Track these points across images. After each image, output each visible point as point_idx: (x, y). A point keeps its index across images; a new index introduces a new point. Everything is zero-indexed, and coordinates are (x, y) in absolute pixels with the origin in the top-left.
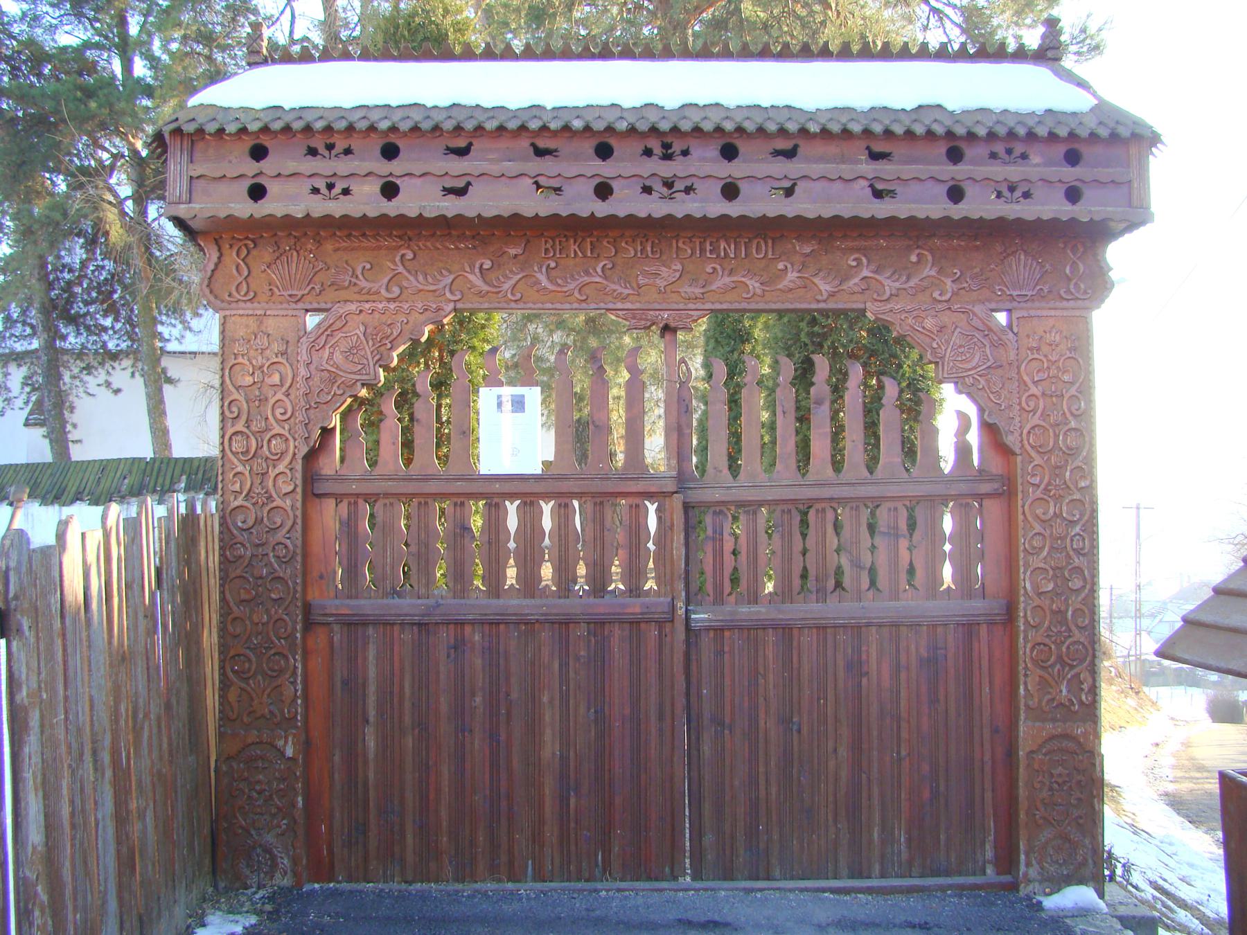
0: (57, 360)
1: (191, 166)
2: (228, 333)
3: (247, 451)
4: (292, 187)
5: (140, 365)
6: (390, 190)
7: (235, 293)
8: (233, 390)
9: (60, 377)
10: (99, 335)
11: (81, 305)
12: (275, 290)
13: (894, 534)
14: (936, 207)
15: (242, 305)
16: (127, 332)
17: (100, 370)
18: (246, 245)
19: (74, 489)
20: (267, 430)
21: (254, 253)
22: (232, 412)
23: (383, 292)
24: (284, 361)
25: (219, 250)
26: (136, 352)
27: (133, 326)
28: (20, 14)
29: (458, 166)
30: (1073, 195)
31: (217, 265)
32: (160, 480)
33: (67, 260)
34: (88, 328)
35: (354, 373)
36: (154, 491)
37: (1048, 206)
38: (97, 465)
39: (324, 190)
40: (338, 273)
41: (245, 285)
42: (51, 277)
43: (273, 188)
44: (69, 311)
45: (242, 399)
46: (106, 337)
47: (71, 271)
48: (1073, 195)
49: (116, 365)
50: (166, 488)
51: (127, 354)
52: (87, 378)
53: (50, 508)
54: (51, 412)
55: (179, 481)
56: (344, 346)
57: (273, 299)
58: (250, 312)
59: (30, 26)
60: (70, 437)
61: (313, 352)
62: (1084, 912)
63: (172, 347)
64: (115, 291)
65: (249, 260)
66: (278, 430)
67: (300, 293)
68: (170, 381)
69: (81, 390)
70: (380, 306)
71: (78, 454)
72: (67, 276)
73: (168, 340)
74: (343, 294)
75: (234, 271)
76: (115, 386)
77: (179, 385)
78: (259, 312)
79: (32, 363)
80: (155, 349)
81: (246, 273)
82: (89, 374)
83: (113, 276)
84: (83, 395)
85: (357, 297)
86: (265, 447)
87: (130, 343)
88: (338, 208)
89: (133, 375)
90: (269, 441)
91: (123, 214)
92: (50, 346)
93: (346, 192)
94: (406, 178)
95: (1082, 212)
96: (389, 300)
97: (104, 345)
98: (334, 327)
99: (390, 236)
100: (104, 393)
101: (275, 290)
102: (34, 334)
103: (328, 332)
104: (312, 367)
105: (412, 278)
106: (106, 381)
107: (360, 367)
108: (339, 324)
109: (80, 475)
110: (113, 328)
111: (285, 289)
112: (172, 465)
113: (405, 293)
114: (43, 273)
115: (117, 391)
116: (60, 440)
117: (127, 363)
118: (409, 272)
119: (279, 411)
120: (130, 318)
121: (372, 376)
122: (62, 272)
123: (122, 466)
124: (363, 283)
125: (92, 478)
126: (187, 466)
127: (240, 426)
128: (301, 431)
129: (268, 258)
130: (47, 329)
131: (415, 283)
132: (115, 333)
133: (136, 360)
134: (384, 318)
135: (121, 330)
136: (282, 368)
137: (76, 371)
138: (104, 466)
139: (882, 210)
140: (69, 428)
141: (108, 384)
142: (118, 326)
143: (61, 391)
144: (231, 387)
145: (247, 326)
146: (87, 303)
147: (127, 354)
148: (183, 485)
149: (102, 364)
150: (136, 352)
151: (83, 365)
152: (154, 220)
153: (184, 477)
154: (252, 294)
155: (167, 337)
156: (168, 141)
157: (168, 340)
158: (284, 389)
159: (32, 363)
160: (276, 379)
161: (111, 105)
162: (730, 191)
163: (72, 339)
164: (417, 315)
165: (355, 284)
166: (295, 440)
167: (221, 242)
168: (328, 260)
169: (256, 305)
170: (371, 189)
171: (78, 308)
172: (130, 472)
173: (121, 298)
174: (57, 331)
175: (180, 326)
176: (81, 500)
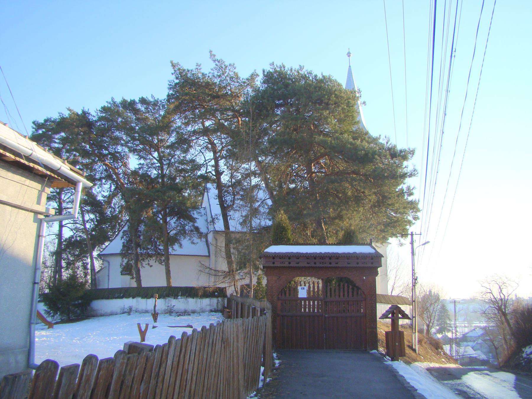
6: (290, 263)
10: (147, 250)
13: (351, 305)
14: (355, 265)
29: (298, 260)
30: (372, 263)
37: (370, 265)
48: (372, 263)
52: (143, 262)
53: (144, 300)
62: (375, 353)
76: (151, 264)
88: (283, 265)
95: (373, 265)
100: (147, 267)
115: (151, 266)
117: (154, 258)
139: (349, 265)
141: (149, 264)
149: (147, 258)
162: (315, 263)
170: (287, 263)
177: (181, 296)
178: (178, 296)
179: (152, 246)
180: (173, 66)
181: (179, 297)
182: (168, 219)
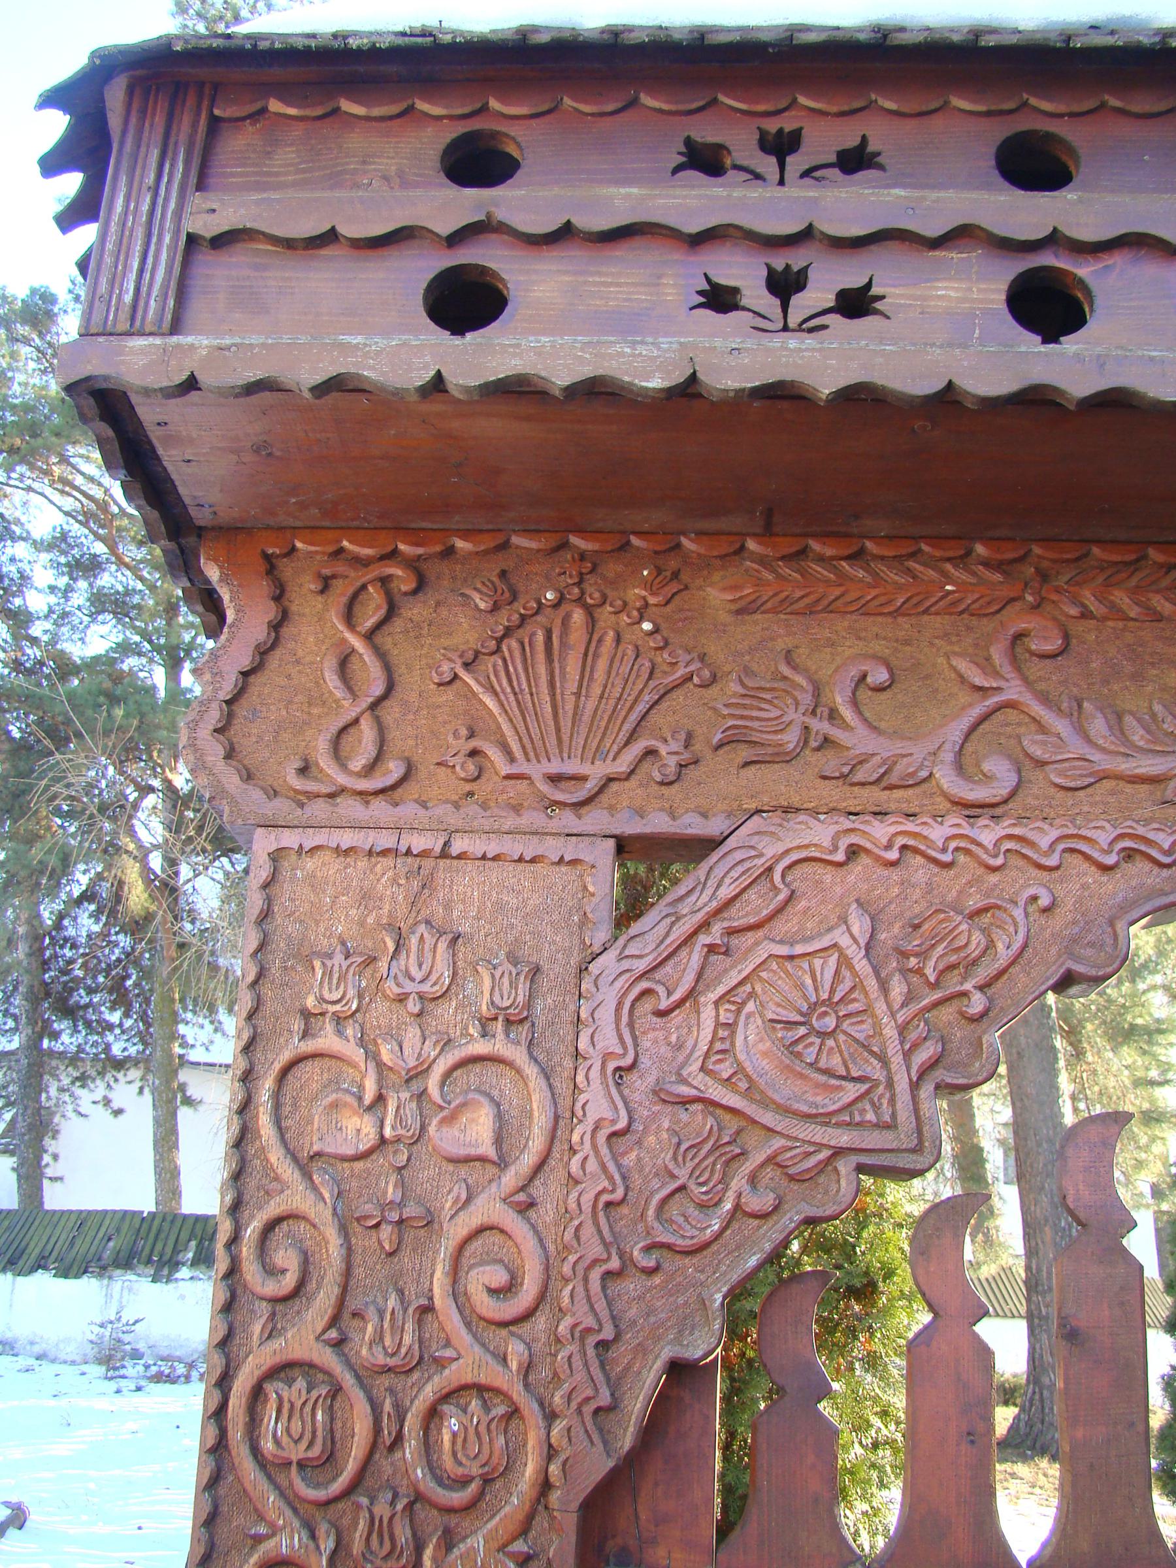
0: (41, 1065)
1: (197, 200)
2: (285, 927)
3: (330, 1459)
4: (623, 279)
5: (150, 1077)
7: (325, 762)
8: (288, 1171)
9: (41, 1089)
11: (82, 991)
12: (494, 754)
15: (350, 808)
16: (140, 1032)
17: (98, 1082)
18: (385, 581)
19: (37, 1251)
20: (424, 1361)
21: (415, 611)
22: (272, 1271)
23: (946, 778)
24: (519, 1055)
25: (279, 596)
26: (147, 1061)
27: (148, 1025)
28: (46, 610)
31: (263, 653)
32: (159, 1246)
33: (71, 932)
34: (88, 1024)
35: (823, 1119)
36: (149, 1261)
38: (73, 1217)
39: (756, 295)
40: (753, 694)
41: (367, 731)
42: (48, 954)
43: (533, 283)
44: (66, 1000)
45: (322, 1214)
46: (110, 1038)
47: (74, 946)
49: (120, 1076)
50: (166, 1257)
51: (135, 1062)
52: (79, 1092)
54: (32, 1139)
55: (186, 1249)
56: (780, 996)
57: (483, 788)
58: (386, 840)
59: (55, 623)
60: (49, 1172)
61: (644, 1017)
63: (194, 1055)
64: (129, 976)
65: (394, 639)
66: (469, 1362)
67: (596, 771)
68: (188, 1101)
69: (70, 1107)
70: (937, 833)
71: (55, 1198)
72: (68, 953)
73: (193, 1046)
74: (774, 782)
75: (332, 680)
76: (116, 1105)
77: (201, 1108)
78: (419, 843)
79: (10, 1068)
80: (170, 1056)
81: (378, 690)
82: (83, 1086)
83: (128, 955)
84: (71, 1114)
85: (832, 793)
86: (411, 1448)
87: (141, 1047)
89: (141, 1090)
90: (433, 1414)
91: (146, 870)
92: (33, 1045)
93: (855, 304)
94: (1117, 260)
96: (972, 810)
97: (108, 1048)
98: (739, 916)
99: (962, 560)
100: (100, 1114)
101: (494, 754)
102: (16, 1029)
103: (715, 935)
104: (640, 1086)
105: (1061, 726)
106: (105, 1097)
107: (852, 1091)
108: (756, 905)
109: (48, 1231)
110: (121, 1025)
111: (533, 752)
112: (178, 1224)
113: (1038, 781)
114: (37, 945)
115: (118, 1112)
116: (31, 1177)
117: (134, 1074)
118: (1045, 699)
119: (482, 1278)
120: (145, 1012)
121: (904, 1137)
122: (62, 947)
123: (107, 1222)
124: (857, 739)
125: (64, 1236)
126: (199, 1226)
127: (303, 1337)
128: (578, 1377)
129: (467, 632)
130: (32, 1022)
131: (1076, 747)
132: (123, 1032)
133: (148, 1070)
134: (950, 885)
135: (131, 1028)
136: (502, 1082)
137: (66, 1081)
138: (83, 1219)
140: (47, 1159)
142: (128, 1023)
143: (41, 1107)
144: (276, 1155)
145: (366, 898)
146: (91, 991)
147: (135, 1062)
148: (190, 1255)
149: (102, 1074)
150: (147, 1061)
151: (76, 1074)
152: (189, 880)
153: (193, 1244)
154: (394, 769)
155: (191, 1041)
156: (115, 122)
157: (193, 1046)
158: (510, 1179)
159: (10, 1068)
160: (477, 1131)
161: (143, 715)
163: (65, 1038)
164: (1092, 876)
165: (827, 742)
166: (551, 1416)
167: (287, 569)
168: (715, 649)
169: (408, 811)
170: (972, 291)
171: (81, 997)
172: (118, 1230)
173: (136, 985)
174: (47, 1023)
175: (209, 1028)
176: (45, 1268)
177: (195, 1263)
178: (175, 1265)
179: (127, 1015)
180: (864, 137)
181: (184, 1272)
182: (185, 871)
